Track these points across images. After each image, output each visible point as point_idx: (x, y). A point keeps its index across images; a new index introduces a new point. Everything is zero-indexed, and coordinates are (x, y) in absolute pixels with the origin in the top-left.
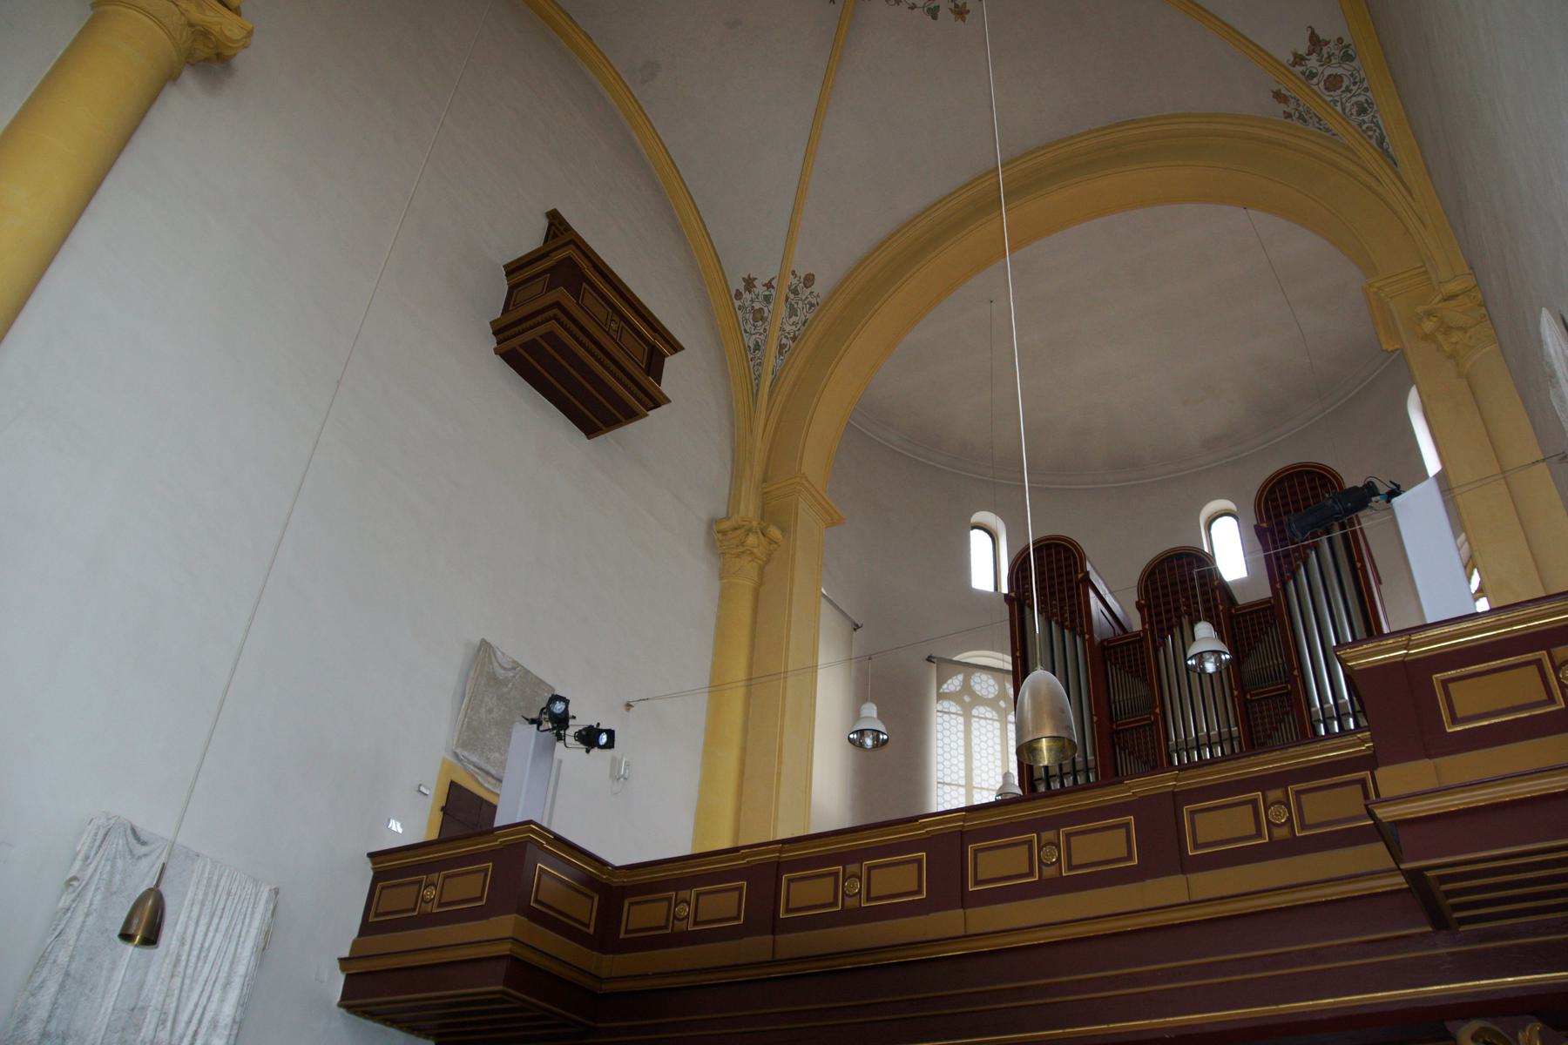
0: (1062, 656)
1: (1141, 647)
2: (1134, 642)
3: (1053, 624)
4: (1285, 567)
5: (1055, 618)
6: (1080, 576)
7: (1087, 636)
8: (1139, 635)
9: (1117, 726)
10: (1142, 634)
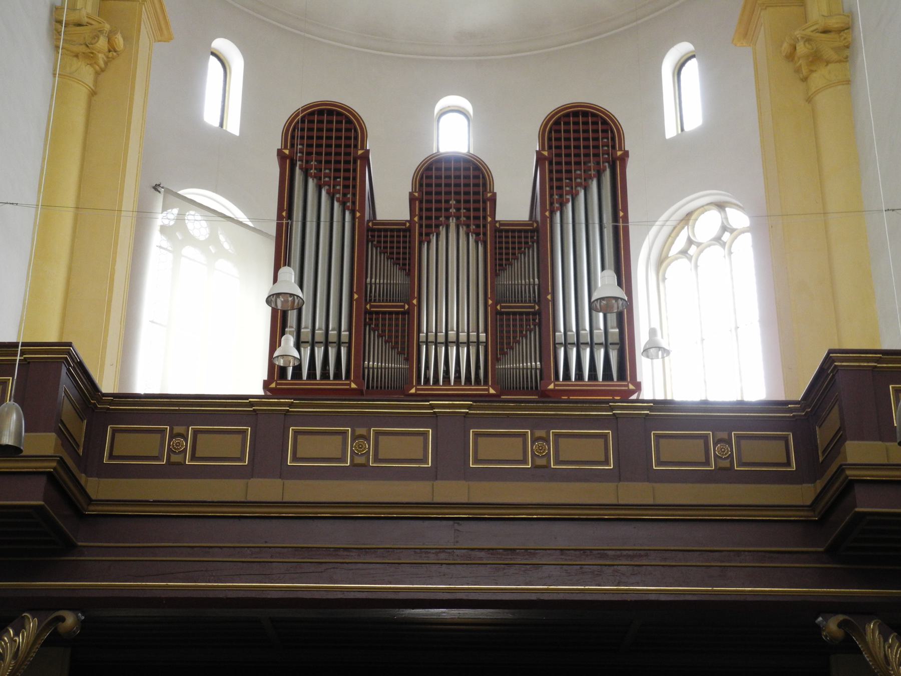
0: (340, 234)
1: (405, 236)
2: (399, 230)
3: (324, 193)
4: (556, 197)
5: (327, 187)
6: (360, 152)
7: (358, 214)
8: (404, 224)
9: (371, 307)
10: (408, 224)
